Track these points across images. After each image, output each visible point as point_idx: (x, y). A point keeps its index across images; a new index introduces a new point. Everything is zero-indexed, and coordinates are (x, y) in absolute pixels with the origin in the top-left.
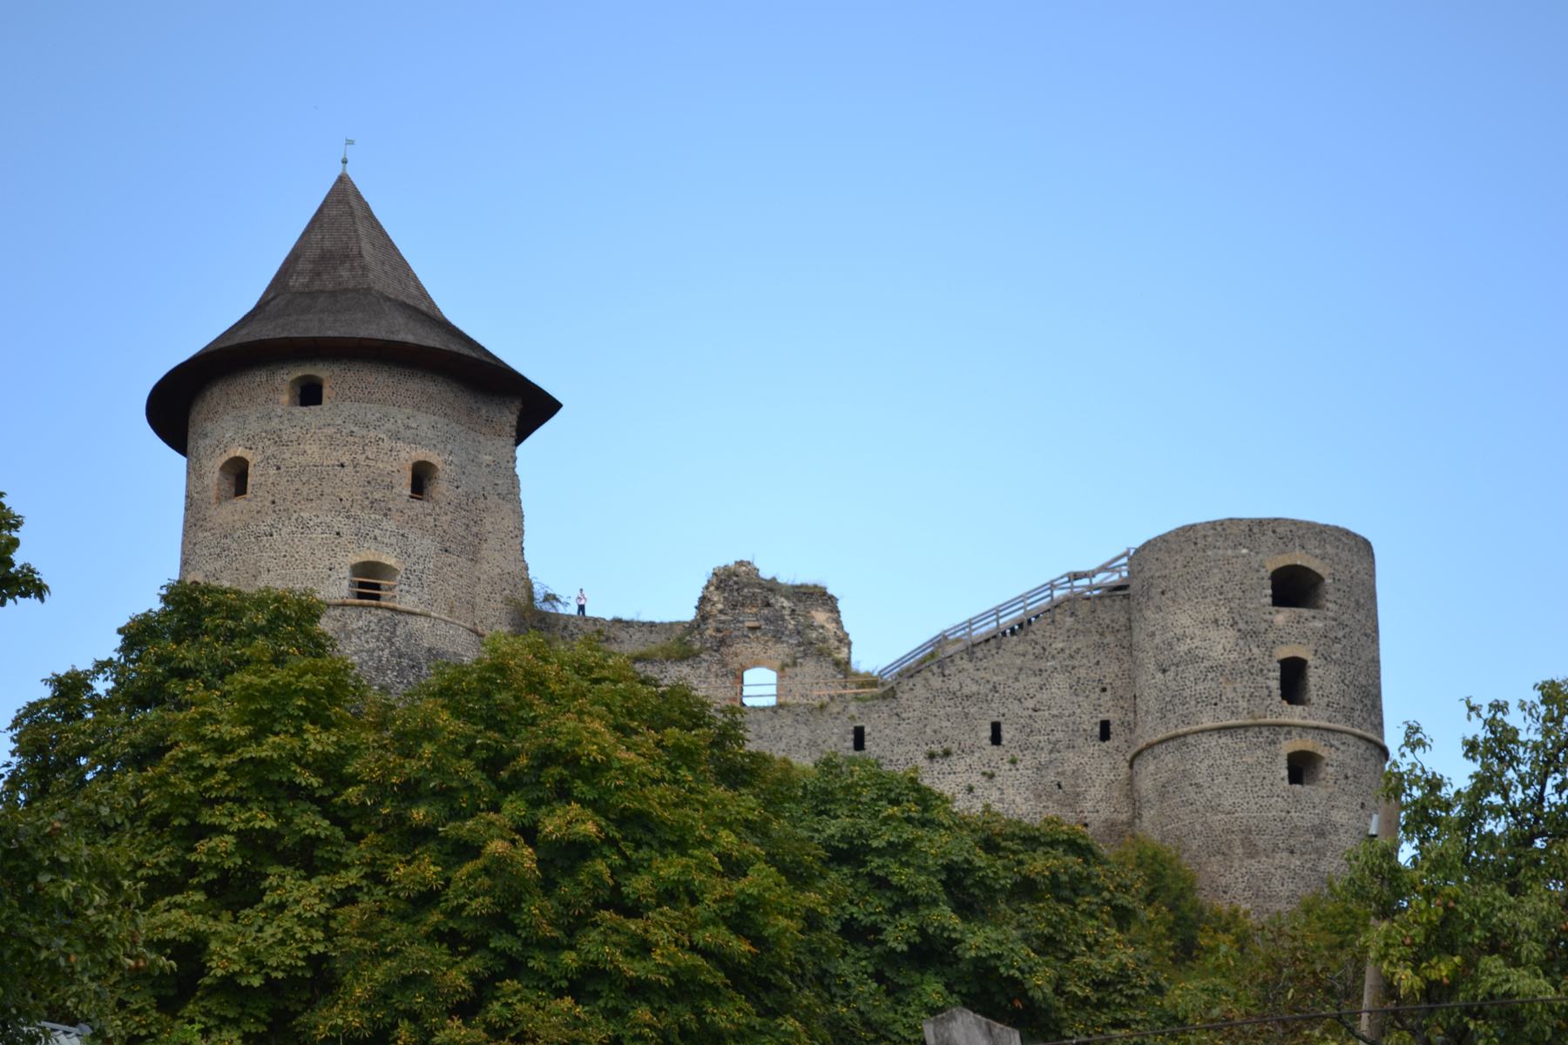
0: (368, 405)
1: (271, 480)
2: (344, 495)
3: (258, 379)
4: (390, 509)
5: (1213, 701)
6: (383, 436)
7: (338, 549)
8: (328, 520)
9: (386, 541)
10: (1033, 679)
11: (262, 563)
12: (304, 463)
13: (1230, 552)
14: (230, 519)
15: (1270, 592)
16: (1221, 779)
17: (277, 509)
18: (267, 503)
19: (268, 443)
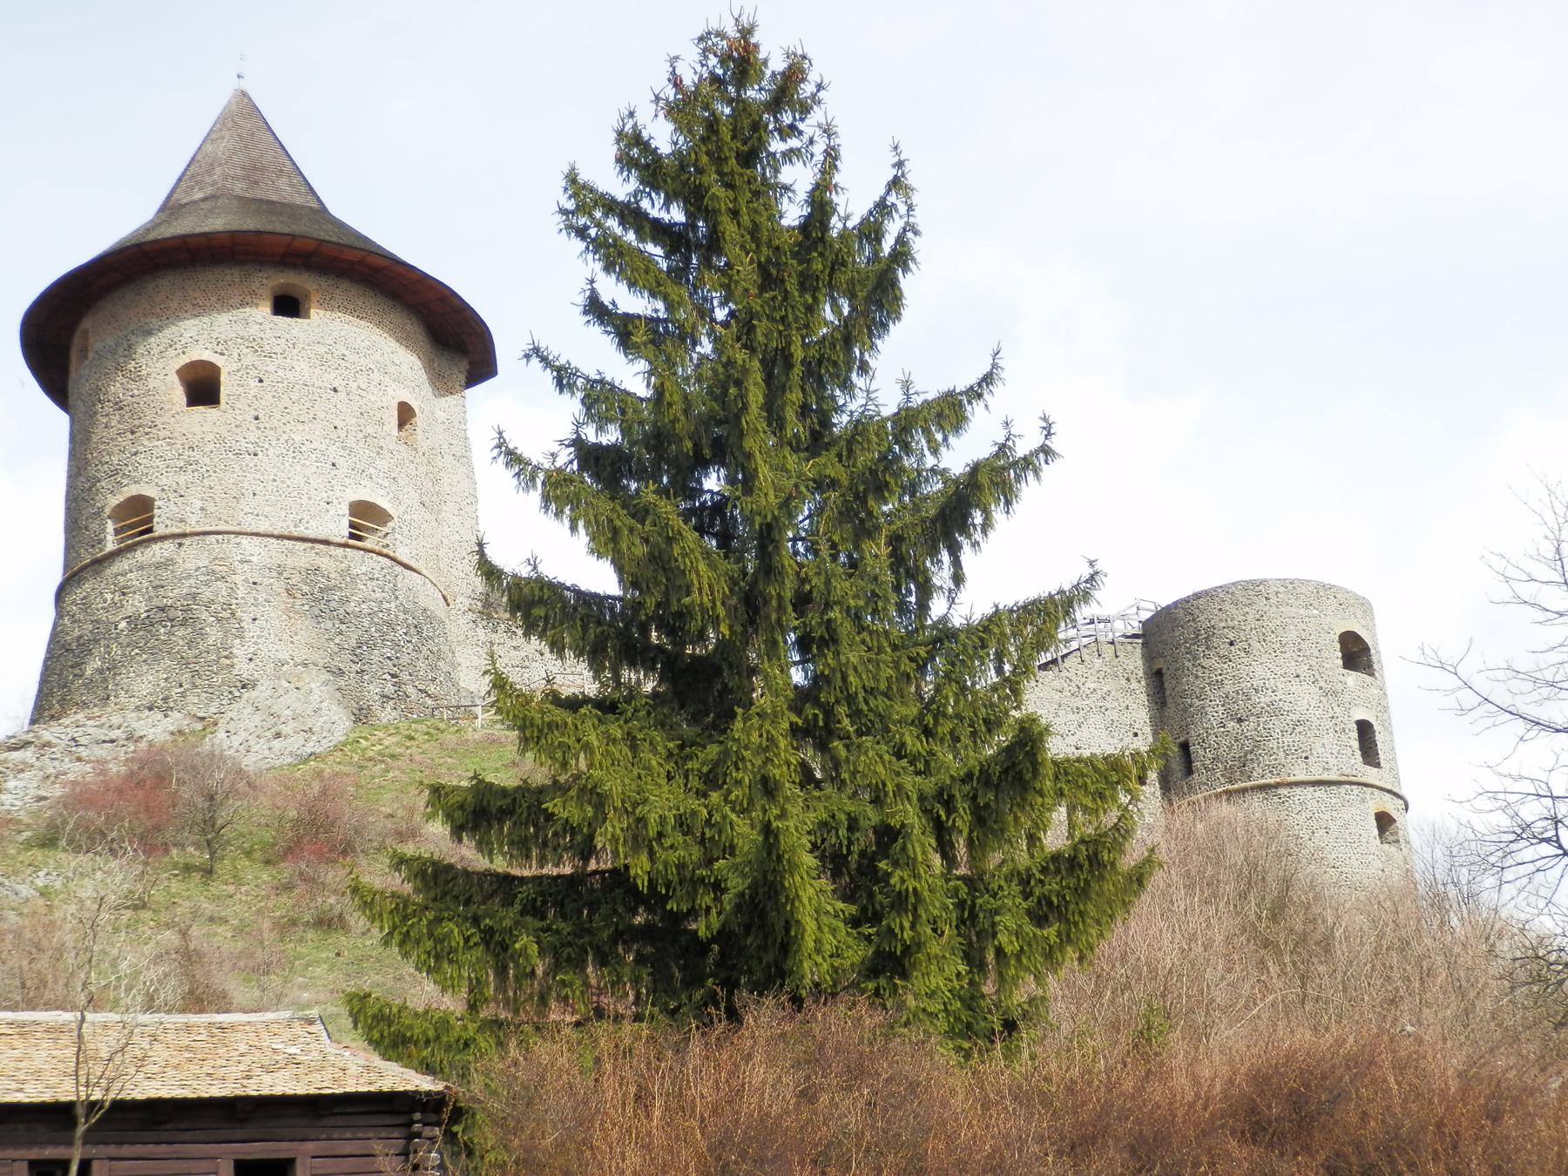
0: (357, 330)
1: (252, 392)
2: (340, 424)
3: (228, 278)
4: (381, 448)
5: (1304, 755)
6: (373, 367)
7: (334, 482)
8: (323, 447)
9: (381, 482)
10: (1071, 717)
11: (246, 485)
12: (292, 380)
13: (1302, 611)
14: (197, 429)
15: (1340, 654)
16: (1322, 832)
17: (261, 426)
18: (250, 418)
19: (246, 351)
